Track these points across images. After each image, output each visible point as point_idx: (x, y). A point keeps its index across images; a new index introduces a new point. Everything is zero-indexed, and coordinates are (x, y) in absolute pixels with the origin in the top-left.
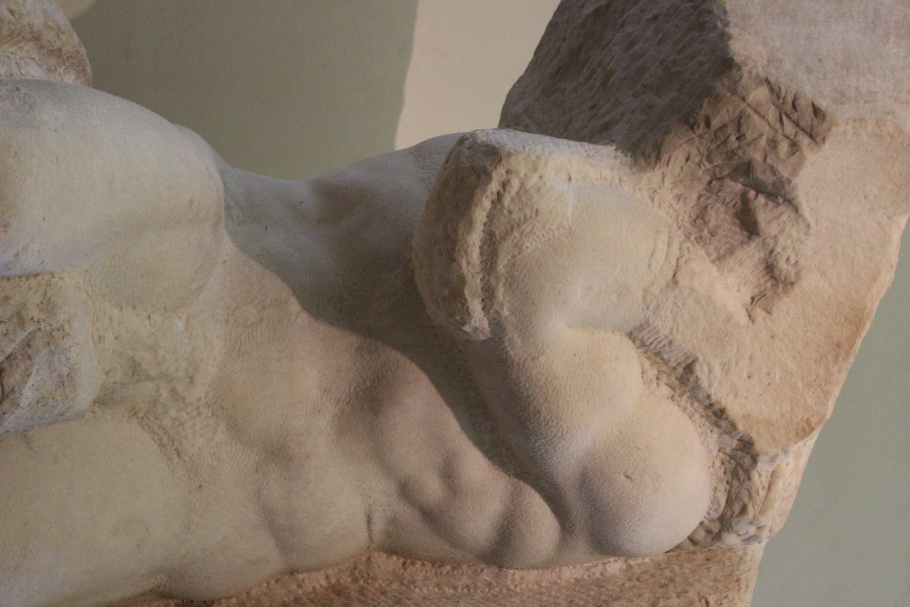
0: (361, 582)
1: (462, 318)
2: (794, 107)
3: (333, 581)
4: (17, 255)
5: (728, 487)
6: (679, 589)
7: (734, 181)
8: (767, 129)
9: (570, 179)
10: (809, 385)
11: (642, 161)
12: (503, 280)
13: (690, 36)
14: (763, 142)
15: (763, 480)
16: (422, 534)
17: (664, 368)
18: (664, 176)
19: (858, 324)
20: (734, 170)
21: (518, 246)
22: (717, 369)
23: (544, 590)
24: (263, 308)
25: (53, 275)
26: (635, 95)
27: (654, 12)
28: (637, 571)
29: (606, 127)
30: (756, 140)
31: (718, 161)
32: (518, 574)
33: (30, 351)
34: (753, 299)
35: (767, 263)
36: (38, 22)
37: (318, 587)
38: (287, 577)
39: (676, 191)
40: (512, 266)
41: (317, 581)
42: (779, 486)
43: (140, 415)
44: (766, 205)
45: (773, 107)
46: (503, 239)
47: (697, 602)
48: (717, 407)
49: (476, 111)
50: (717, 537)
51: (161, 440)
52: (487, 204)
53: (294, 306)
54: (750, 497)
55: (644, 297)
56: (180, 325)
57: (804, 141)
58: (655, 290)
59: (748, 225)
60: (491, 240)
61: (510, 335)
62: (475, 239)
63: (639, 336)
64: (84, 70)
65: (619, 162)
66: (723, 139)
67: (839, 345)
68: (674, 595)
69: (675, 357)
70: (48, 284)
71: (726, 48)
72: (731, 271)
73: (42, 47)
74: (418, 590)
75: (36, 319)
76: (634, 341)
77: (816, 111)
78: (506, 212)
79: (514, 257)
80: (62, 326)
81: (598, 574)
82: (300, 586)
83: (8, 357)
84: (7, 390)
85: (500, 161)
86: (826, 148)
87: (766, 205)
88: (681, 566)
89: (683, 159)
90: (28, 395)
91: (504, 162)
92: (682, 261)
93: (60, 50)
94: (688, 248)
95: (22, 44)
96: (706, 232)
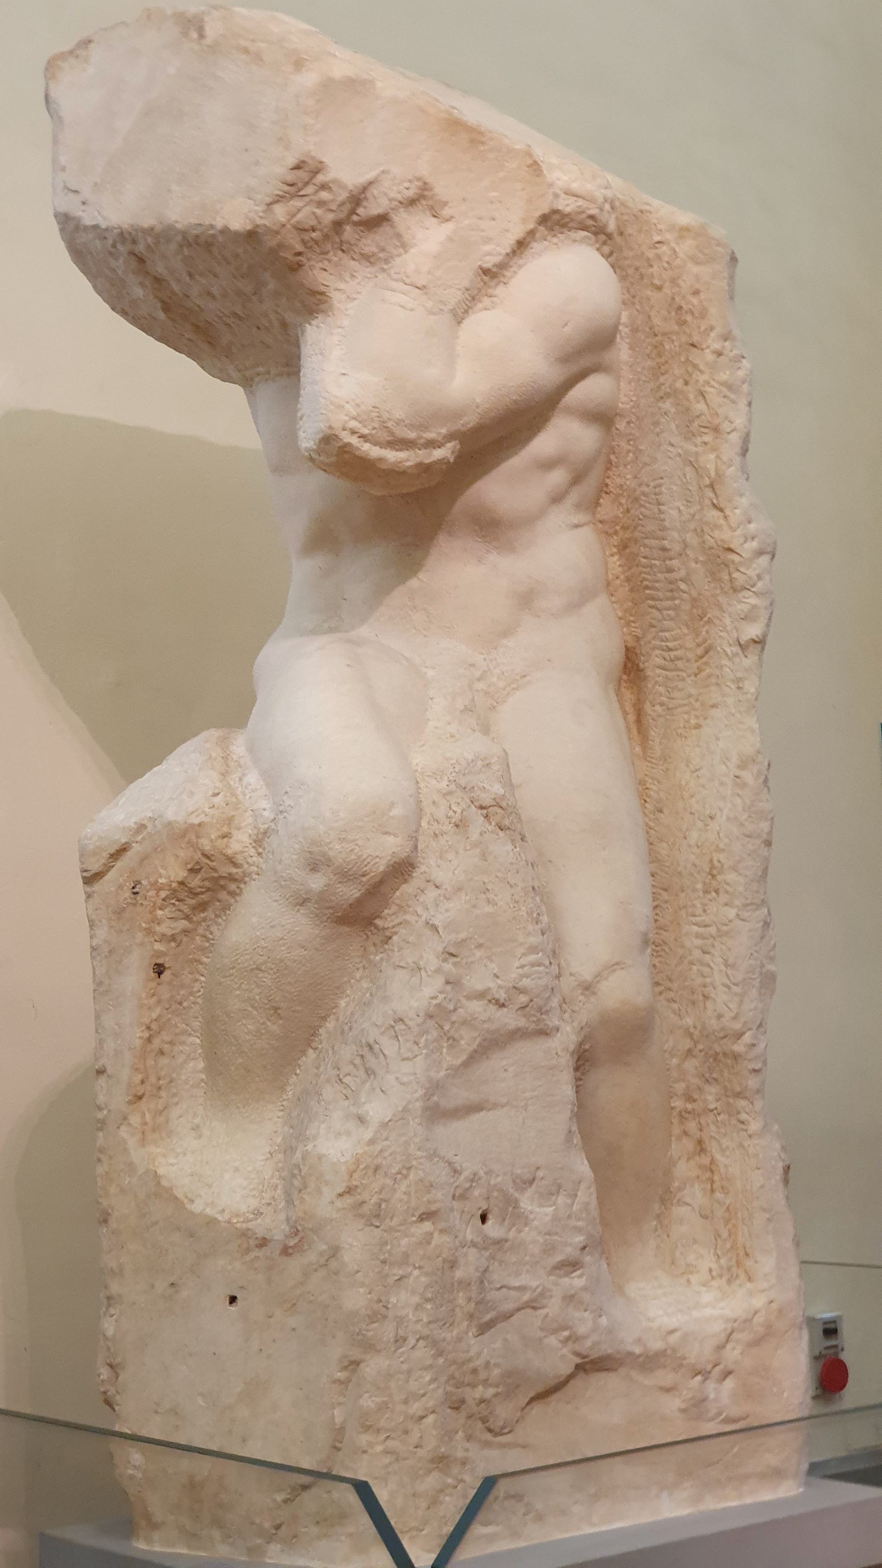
0: (618, 528)
2: (292, 185)
8: (308, 208)
11: (322, 306)
14: (319, 212)
16: (592, 484)
21: (398, 422)
22: (487, 248)
23: (636, 377)
29: (284, 325)
30: (317, 217)
33: (468, 787)
34: (435, 216)
39: (348, 279)
40: (412, 427)
42: (575, 186)
44: (365, 207)
45: (291, 202)
46: (393, 434)
47: (657, 251)
52: (366, 447)
53: (414, 583)
54: (583, 212)
55: (434, 314)
57: (320, 178)
58: (429, 304)
59: (381, 220)
60: (392, 443)
62: (392, 456)
63: (459, 315)
65: (322, 325)
68: (651, 270)
70: (422, 773)
71: (237, 234)
77: (297, 167)
79: (406, 426)
81: (627, 330)
83: (472, 802)
84: (493, 803)
88: (626, 258)
89: (324, 274)
92: (407, 281)
96: (381, 255)
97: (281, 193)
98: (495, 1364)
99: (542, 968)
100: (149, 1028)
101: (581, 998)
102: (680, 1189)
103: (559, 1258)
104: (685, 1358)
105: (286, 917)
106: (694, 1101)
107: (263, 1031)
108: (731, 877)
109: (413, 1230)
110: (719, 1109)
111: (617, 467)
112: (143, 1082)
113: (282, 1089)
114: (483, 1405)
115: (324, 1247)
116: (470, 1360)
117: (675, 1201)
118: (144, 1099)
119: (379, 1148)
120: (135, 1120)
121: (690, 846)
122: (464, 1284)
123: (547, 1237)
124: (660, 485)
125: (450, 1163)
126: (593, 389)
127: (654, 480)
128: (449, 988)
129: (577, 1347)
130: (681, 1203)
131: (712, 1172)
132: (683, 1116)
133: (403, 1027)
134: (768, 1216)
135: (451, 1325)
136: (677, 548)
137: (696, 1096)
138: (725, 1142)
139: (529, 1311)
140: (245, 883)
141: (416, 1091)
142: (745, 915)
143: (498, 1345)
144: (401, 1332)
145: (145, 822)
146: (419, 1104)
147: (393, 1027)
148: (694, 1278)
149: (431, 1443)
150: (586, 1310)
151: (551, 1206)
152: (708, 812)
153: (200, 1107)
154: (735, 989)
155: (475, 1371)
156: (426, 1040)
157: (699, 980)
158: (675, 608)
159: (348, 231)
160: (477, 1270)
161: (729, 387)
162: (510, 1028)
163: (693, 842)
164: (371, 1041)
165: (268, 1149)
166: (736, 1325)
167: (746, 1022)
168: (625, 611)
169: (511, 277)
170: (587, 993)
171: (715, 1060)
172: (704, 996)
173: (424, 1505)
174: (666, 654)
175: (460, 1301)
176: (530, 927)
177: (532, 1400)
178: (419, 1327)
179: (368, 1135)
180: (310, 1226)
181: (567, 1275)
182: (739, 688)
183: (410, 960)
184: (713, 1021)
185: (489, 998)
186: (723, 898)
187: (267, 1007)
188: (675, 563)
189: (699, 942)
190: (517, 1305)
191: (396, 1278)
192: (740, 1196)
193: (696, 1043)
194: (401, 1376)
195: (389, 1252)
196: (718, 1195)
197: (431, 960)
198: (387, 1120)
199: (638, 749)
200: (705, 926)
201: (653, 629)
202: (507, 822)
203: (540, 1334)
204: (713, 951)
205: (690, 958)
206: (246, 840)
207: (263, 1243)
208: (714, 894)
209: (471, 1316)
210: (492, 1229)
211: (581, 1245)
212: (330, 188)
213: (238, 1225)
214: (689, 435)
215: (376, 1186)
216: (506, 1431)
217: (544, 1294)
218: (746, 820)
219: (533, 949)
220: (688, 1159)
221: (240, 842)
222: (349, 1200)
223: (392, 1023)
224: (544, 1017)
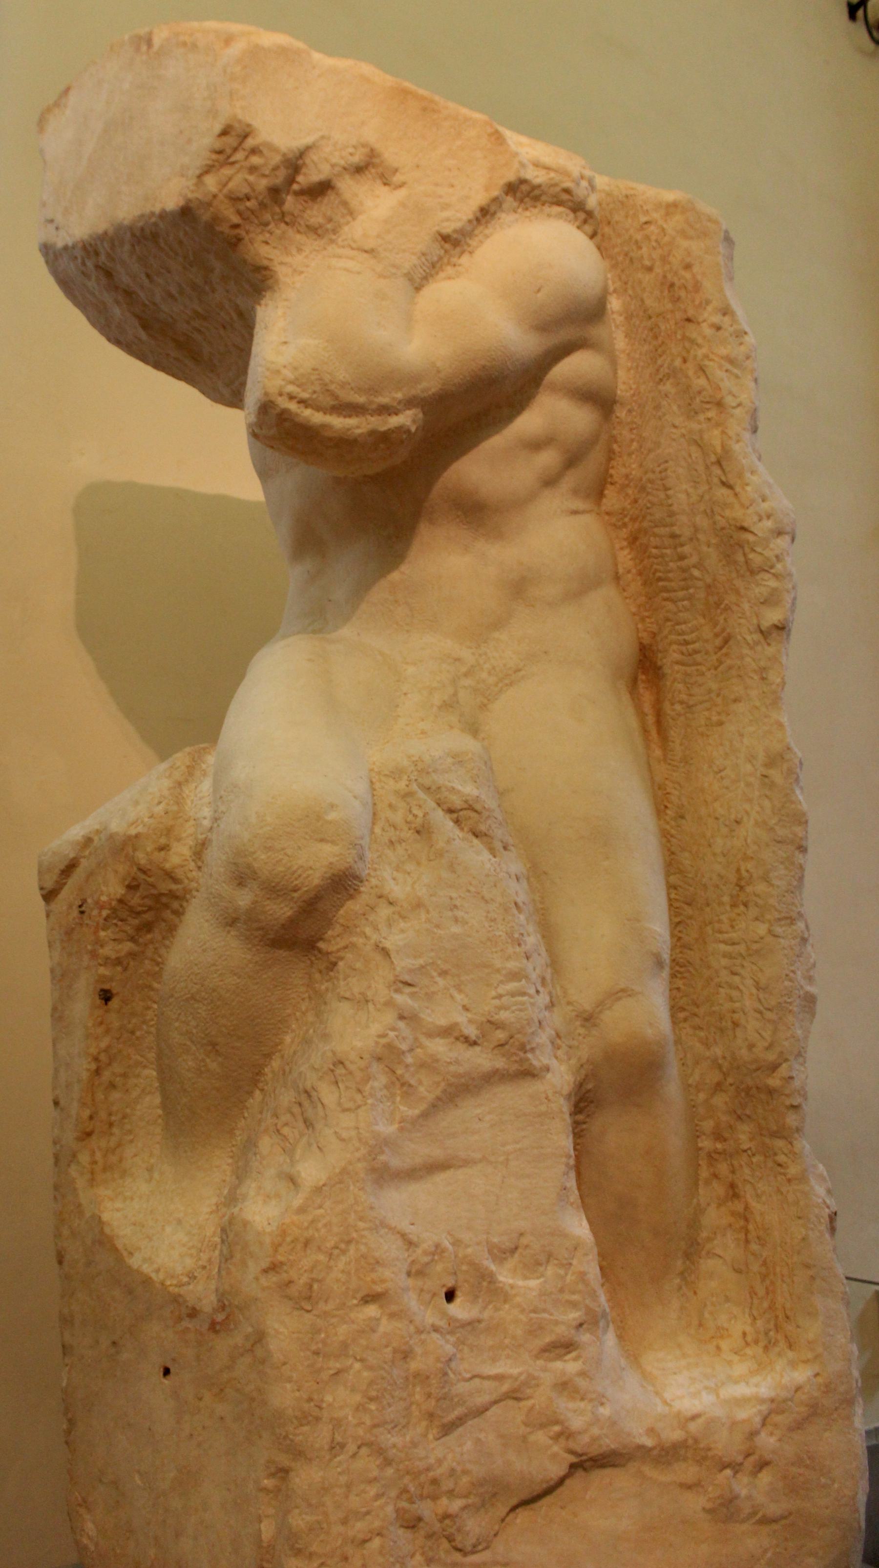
0: (626, 520)
1: (405, 432)
4: (355, 797)
5: (547, 205)
6: (634, 247)
9: (285, 343)
12: (372, 398)
13: (162, 245)
14: (251, 178)
16: (590, 468)
17: (445, 260)
18: (281, 263)
19: (405, 92)
20: (276, 202)
21: (343, 385)
23: (635, 364)
24: (396, 601)
25: (372, 770)
26: (213, 291)
27: (144, 277)
28: (618, 284)
29: (241, 315)
30: (250, 185)
31: (268, 217)
32: (621, 386)
33: (434, 788)
34: (385, 184)
36: (166, 783)
37: (630, 557)
38: (621, 582)
39: (294, 251)
40: (359, 390)
41: (625, 558)
42: (547, 160)
43: (485, 701)
44: (305, 174)
46: (337, 398)
48: (479, 214)
49: (233, 425)
50: (590, 214)
51: (507, 685)
52: (307, 413)
53: (395, 576)
54: (556, 185)
55: (385, 277)
56: (411, 670)
57: (250, 142)
59: (322, 189)
61: (419, 392)
62: (338, 422)
63: (418, 281)
64: (204, 749)
68: (640, 252)
69: (437, 251)
70: (379, 773)
71: (172, 213)
72: (361, 203)
73: (187, 781)
74: (634, 473)
75: (407, 783)
77: (224, 133)
78: (315, 396)
79: (352, 389)
80: (413, 762)
82: (629, 572)
83: (439, 805)
84: (466, 806)
85: (271, 402)
86: (256, 123)
87: (305, 174)
90: (469, 790)
91: (273, 399)
92: (354, 245)
93: (188, 767)
94: (343, 241)
95: (185, 796)
96: (329, 226)
99: (525, 998)
100: (96, 1059)
101: (582, 1031)
102: (709, 1239)
104: (709, 1449)
105: (217, 940)
106: (725, 1140)
107: (203, 1069)
108: (760, 887)
109: (352, 1315)
110: (754, 1150)
111: (620, 457)
112: (91, 1118)
113: (231, 1133)
115: (250, 1330)
117: (703, 1253)
118: (94, 1137)
119: (310, 1218)
120: (84, 1158)
121: (714, 854)
122: (421, 1378)
123: (532, 1315)
124: (666, 470)
125: (403, 1235)
126: (579, 365)
127: (659, 466)
128: (401, 1024)
129: (572, 1445)
130: (710, 1254)
131: (746, 1220)
132: (712, 1157)
133: (343, 1071)
135: (404, 1427)
136: (687, 532)
138: (761, 1186)
139: (510, 1402)
140: (187, 901)
141: (358, 1150)
143: (469, 1445)
144: (338, 1438)
145: (92, 836)
147: (332, 1071)
148: (725, 1345)
151: (538, 1278)
152: (733, 817)
153: (158, 1146)
154: (769, 1015)
155: (435, 1482)
157: (728, 1005)
158: (690, 598)
159: (290, 202)
161: (731, 361)
163: (718, 850)
164: (309, 1087)
165: (214, 1200)
168: (639, 606)
169: (477, 247)
171: (747, 1094)
172: (733, 1022)
174: (684, 648)
175: (417, 1397)
176: (510, 950)
177: (514, 1509)
178: (361, 1432)
179: (297, 1202)
180: (236, 1303)
181: (559, 1357)
183: (356, 990)
185: (456, 1034)
186: (753, 912)
187: (205, 1041)
188: (687, 549)
189: (724, 962)
190: (494, 1397)
191: (332, 1372)
192: (779, 1249)
193: (725, 1075)
194: (338, 1491)
195: (324, 1342)
196: (754, 1247)
197: (380, 989)
198: (321, 1183)
199: (658, 753)
200: (733, 944)
201: (669, 624)
203: (523, 1430)
204: (742, 972)
205: (716, 980)
206: (186, 852)
207: (193, 1313)
208: (742, 908)
209: (431, 1416)
210: (458, 1309)
212: (261, 152)
213: (171, 1289)
214: (691, 413)
215: (306, 1263)
216: (480, 1547)
217: (531, 1381)
218: (776, 824)
220: (719, 1206)
221: (179, 855)
222: (274, 1278)
223: (332, 1067)
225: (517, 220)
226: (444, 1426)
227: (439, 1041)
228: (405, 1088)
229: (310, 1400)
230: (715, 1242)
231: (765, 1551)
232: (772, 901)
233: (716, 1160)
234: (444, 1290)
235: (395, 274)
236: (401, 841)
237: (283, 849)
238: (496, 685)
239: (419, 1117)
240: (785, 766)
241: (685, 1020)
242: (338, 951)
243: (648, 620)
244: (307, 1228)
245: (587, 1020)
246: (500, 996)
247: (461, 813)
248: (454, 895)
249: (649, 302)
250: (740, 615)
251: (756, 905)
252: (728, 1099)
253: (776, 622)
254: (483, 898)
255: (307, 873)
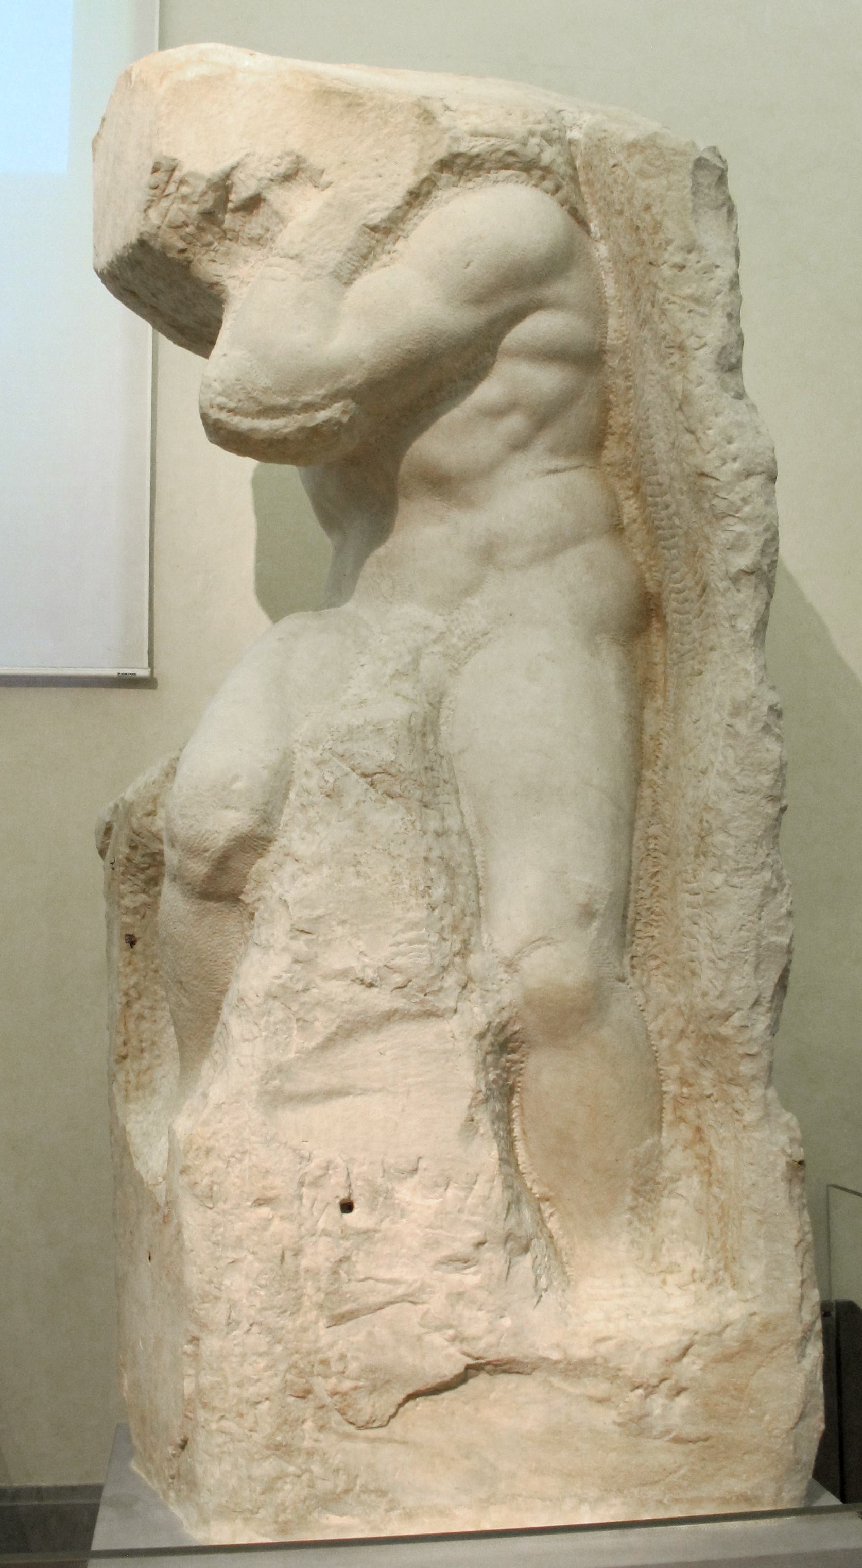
0: (630, 469)
1: (334, 425)
2: (156, 188)
3: (631, 493)
5: (492, 171)
7: (224, 221)
8: (175, 206)
10: (386, 123)
14: (184, 206)
15: (479, 143)
17: (379, 250)
21: (265, 390)
22: (373, 205)
32: (611, 334)
34: (315, 186)
35: (283, 181)
37: (636, 505)
40: (283, 393)
46: (260, 403)
50: (547, 171)
51: (475, 648)
53: (381, 551)
55: (310, 279)
57: (177, 175)
59: (253, 204)
63: (346, 276)
66: (191, 238)
67: (349, 105)
70: (302, 744)
72: (291, 210)
76: (355, 279)
77: (155, 170)
78: (240, 405)
82: (635, 521)
86: (181, 156)
97: (150, 198)
98: (353, 1357)
100: (126, 994)
101: (505, 976)
102: (673, 1180)
103: (445, 1252)
108: (719, 838)
109: (247, 1215)
111: (617, 406)
112: (125, 1044)
114: (336, 1397)
116: (316, 1352)
118: (128, 1060)
121: (686, 805)
122: (313, 1273)
123: (428, 1230)
128: (298, 967)
129: (466, 1348)
132: (679, 1102)
134: (759, 1217)
137: (691, 1081)
138: (723, 1132)
141: (252, 1075)
142: (736, 880)
143: (360, 1337)
146: (255, 1088)
148: (671, 1279)
149: (267, 1428)
150: (480, 1309)
151: (437, 1198)
154: (723, 965)
155: (325, 1362)
156: (267, 1022)
159: (229, 220)
160: (327, 1259)
162: (381, 1009)
166: (697, 1337)
167: (733, 1002)
169: (413, 230)
170: (509, 970)
171: (705, 1041)
173: (259, 1489)
178: (252, 1312)
181: (457, 1270)
182: (733, 626)
184: (699, 999)
185: (352, 977)
186: (711, 862)
189: (688, 911)
190: (387, 1298)
191: (231, 1261)
194: (234, 1359)
195: (222, 1234)
196: (715, 1190)
202: (397, 789)
203: (418, 1330)
208: (702, 858)
209: (321, 1306)
211: (476, 1241)
215: (207, 1168)
216: (375, 1425)
218: (739, 774)
219: (414, 925)
220: (686, 1148)
224: (430, 997)
225: (457, 194)
226: (333, 1317)
227: (334, 982)
228: (300, 1023)
229: (210, 1282)
230: (680, 1183)
231: (680, 1467)
232: (730, 852)
233: (683, 1104)
234: (338, 1201)
235: (319, 275)
236: (312, 804)
237: (194, 816)
238: (465, 649)
239: (314, 1049)
240: (750, 715)
241: (657, 968)
242: (254, 902)
243: (654, 569)
244: (209, 1138)
245: (509, 965)
246: (399, 944)
247: (375, 777)
248: (358, 852)
249: (624, 247)
250: (711, 562)
251: (714, 856)
252: (690, 1046)
253: (743, 568)
254: (389, 854)
255: (213, 836)
